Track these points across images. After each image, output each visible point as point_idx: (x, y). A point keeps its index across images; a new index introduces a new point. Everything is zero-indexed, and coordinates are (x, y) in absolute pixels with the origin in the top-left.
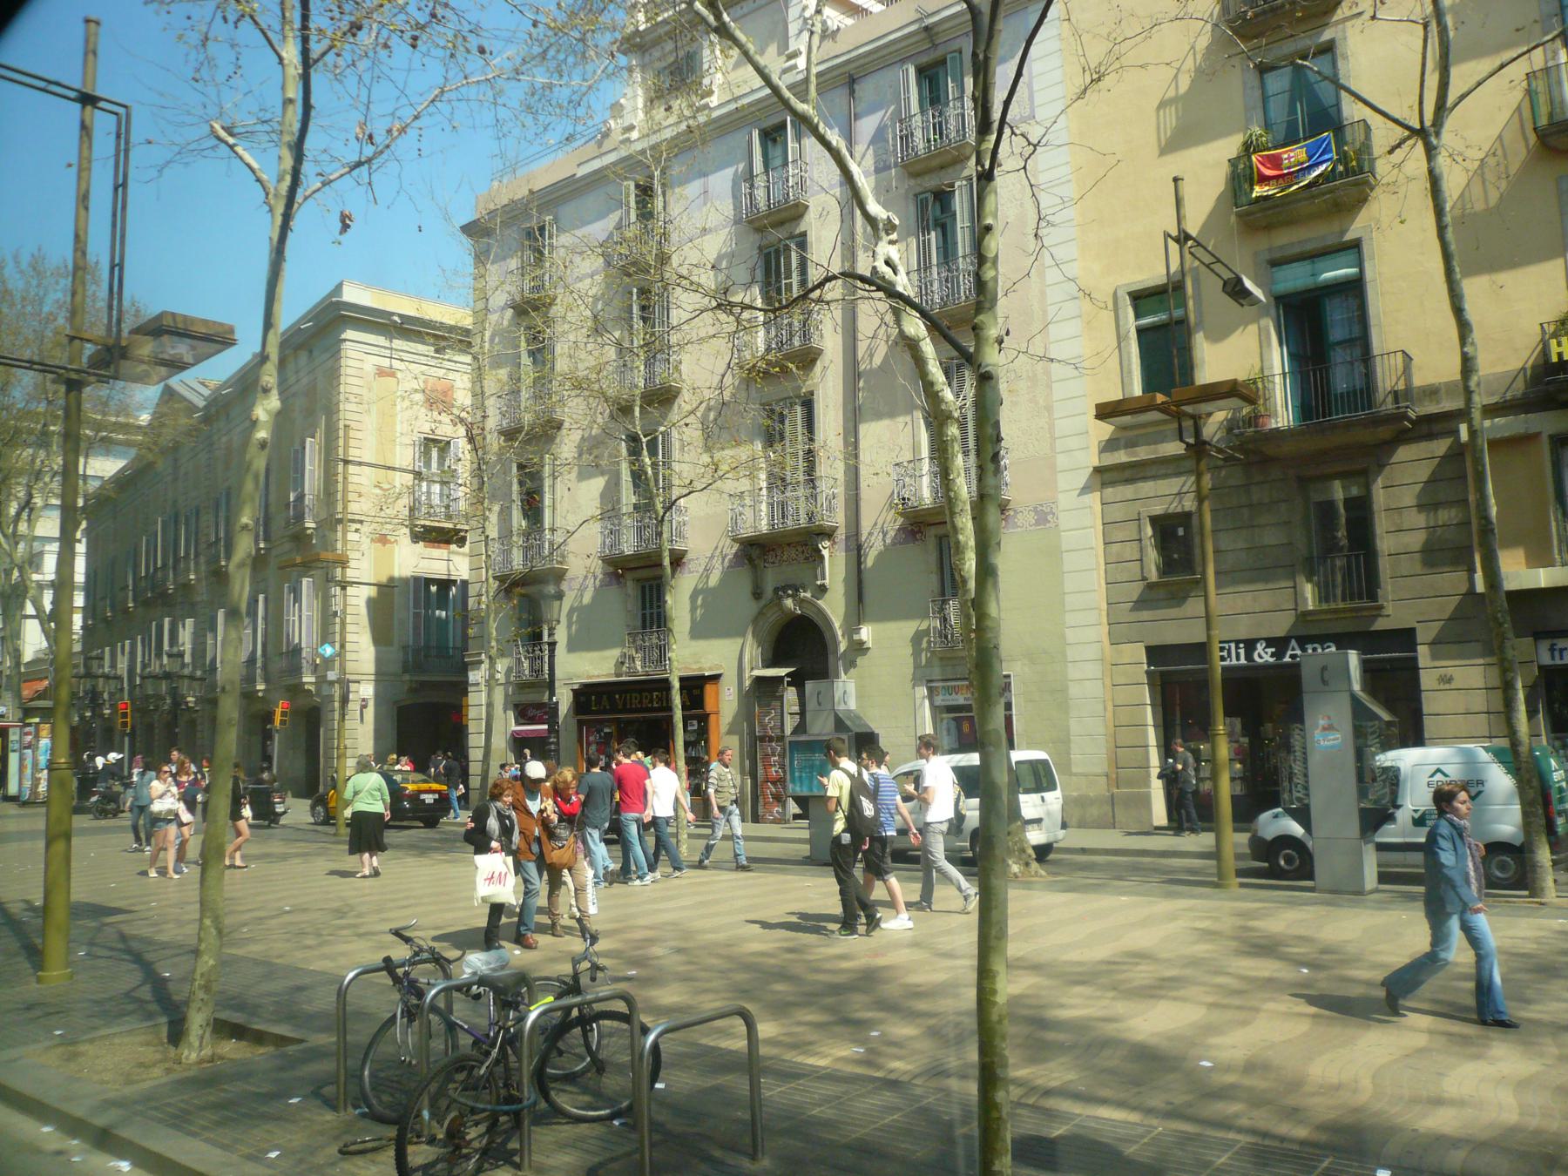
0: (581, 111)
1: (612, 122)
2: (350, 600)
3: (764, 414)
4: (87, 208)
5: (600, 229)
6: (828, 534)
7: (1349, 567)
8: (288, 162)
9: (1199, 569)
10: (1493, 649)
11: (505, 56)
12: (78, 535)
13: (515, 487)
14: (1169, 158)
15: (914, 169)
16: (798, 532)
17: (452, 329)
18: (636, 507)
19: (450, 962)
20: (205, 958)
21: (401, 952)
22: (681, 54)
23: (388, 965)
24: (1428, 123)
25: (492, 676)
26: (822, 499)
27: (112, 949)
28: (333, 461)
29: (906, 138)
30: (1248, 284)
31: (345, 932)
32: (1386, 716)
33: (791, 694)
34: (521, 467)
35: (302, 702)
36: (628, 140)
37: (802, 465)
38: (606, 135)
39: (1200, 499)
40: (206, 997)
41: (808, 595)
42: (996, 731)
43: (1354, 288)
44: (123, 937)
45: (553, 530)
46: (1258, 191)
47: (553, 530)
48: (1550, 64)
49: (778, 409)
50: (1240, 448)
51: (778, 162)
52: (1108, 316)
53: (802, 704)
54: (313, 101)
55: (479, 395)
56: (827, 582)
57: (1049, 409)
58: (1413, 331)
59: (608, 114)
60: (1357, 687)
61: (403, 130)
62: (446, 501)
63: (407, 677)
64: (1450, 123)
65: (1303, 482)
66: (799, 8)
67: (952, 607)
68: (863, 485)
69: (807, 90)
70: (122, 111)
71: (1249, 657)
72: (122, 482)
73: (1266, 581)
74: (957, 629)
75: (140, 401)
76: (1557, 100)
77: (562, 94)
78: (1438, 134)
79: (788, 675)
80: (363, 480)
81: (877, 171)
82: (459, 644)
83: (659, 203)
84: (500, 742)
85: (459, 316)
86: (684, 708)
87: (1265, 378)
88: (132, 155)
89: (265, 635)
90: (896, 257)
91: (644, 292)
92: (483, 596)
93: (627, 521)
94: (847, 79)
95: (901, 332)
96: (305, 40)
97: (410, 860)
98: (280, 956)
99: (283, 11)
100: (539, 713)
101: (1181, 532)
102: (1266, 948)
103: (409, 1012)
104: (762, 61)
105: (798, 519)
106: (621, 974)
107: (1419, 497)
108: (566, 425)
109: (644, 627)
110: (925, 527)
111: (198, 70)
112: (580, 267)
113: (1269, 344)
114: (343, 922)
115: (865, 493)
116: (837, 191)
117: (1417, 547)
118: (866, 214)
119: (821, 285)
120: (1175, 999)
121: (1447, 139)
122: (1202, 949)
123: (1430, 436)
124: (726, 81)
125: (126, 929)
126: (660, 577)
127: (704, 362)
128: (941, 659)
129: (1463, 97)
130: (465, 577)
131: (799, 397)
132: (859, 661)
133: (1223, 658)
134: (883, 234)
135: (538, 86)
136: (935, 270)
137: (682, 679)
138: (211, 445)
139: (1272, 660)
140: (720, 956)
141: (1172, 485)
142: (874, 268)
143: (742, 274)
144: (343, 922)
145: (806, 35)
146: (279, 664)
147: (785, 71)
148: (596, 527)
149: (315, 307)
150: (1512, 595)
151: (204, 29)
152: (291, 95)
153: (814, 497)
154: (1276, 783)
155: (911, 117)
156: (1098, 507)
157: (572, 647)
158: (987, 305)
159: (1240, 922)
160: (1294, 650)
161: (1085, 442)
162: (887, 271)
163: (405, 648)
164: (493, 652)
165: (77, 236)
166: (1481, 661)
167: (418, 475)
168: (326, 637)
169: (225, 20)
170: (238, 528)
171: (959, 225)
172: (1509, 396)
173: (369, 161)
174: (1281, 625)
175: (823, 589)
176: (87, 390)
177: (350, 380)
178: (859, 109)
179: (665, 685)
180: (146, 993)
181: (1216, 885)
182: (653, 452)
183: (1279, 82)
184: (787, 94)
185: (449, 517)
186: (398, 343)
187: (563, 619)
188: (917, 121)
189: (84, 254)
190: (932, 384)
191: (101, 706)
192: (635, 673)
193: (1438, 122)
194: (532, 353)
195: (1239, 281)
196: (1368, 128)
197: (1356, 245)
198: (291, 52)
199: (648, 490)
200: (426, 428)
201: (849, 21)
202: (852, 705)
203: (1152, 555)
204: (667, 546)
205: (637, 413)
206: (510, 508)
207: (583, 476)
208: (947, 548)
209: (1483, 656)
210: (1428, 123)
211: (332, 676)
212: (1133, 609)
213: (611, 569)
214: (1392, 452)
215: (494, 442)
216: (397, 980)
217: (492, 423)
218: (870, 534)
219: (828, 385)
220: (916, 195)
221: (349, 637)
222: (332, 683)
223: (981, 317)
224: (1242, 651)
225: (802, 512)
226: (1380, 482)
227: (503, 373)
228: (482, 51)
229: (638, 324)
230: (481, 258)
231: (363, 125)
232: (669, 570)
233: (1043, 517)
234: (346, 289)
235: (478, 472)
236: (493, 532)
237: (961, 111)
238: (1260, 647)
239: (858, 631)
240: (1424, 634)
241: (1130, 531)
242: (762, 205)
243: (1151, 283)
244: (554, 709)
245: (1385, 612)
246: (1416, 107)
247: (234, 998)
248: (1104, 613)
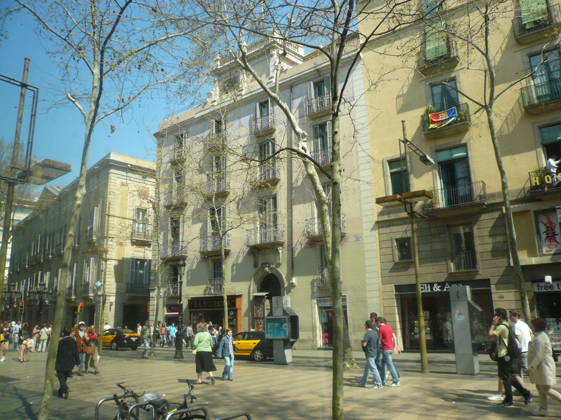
0: (197, 95)
2: (108, 266)
4: (21, 123)
6: (281, 244)
7: (466, 257)
8: (93, 107)
9: (413, 258)
10: (518, 287)
11: (172, 73)
12: (9, 241)
13: (169, 225)
14: (400, 115)
15: (313, 117)
17: (148, 169)
19: (139, 397)
20: (46, 395)
21: (120, 393)
22: (232, 77)
23: (115, 398)
24: (487, 104)
25: (159, 294)
26: (279, 232)
27: (11, 393)
28: (104, 215)
29: (310, 106)
30: (428, 157)
31: (100, 388)
32: (480, 309)
33: (267, 302)
34: (172, 218)
35: (88, 303)
36: (213, 105)
37: (272, 219)
38: (206, 103)
39: (413, 232)
40: (46, 410)
41: (274, 266)
42: (339, 308)
43: (465, 160)
44: (15, 389)
45: (183, 242)
46: (432, 126)
48: (528, 85)
49: (264, 199)
50: (427, 215)
51: (265, 114)
52: (380, 167)
54: (103, 87)
55: (158, 193)
56: (281, 261)
57: (360, 201)
58: (485, 175)
60: (469, 299)
61: (134, 98)
62: (144, 230)
63: (127, 295)
64: (495, 104)
65: (449, 226)
66: (274, 62)
67: (326, 271)
68: (294, 227)
70: (35, 90)
71: (431, 289)
72: (26, 222)
74: (327, 279)
75: (35, 192)
76: (531, 97)
78: (491, 107)
79: (266, 295)
80: (115, 222)
81: (300, 117)
82: (147, 283)
83: (223, 127)
84: (161, 318)
85: (151, 165)
86: (228, 307)
87: (435, 190)
88: (38, 104)
89: (76, 279)
90: (306, 146)
91: (218, 158)
92: (156, 266)
93: (210, 239)
94: (290, 86)
95: (308, 172)
96: (102, 66)
97: (125, 361)
98: (74, 397)
99: (94, 56)
101: (407, 244)
102: (440, 394)
103: (122, 415)
104: (260, 79)
105: (270, 239)
106: (202, 403)
107: (489, 232)
109: (215, 277)
110: (315, 242)
111: (63, 77)
112: (195, 149)
113: (436, 179)
114: (99, 384)
117: (490, 250)
118: (296, 132)
119: (279, 152)
120: (406, 412)
121: (494, 109)
122: (416, 394)
123: (493, 211)
124: (248, 86)
125: (17, 386)
129: (499, 95)
130: (150, 258)
133: (422, 290)
134: (301, 138)
136: (320, 152)
138: (60, 209)
139: (440, 290)
140: (240, 397)
141: (404, 227)
143: (252, 150)
144: (99, 384)
145: (276, 71)
146: (81, 289)
147: (268, 83)
148: (198, 241)
150: (524, 267)
151: (67, 62)
152: (95, 85)
153: (276, 231)
154: (442, 335)
156: (377, 235)
157: (188, 284)
158: (336, 159)
159: (430, 385)
160: (447, 286)
161: (372, 212)
165: (17, 132)
166: (513, 291)
167: (134, 221)
168: (98, 279)
169: (74, 59)
170: (68, 235)
171: (328, 136)
172: (519, 197)
173: (122, 108)
174: (443, 278)
175: (279, 265)
176: (16, 187)
177: (112, 181)
179: (222, 298)
180: (23, 410)
181: (422, 372)
182: (219, 214)
183: (437, 90)
184: (268, 90)
185: (145, 236)
186: (129, 174)
187: (185, 273)
188: (314, 101)
189: (19, 138)
190: (318, 191)
191: (13, 303)
192: (211, 294)
193: (491, 103)
194: (177, 179)
195: (425, 156)
196: (468, 106)
197: (465, 145)
198: (97, 71)
200: (138, 205)
201: (291, 67)
203: (397, 253)
204: (223, 248)
205: (214, 200)
207: (194, 223)
208: (323, 248)
209: (514, 289)
210: (487, 104)
211: (100, 293)
212: (390, 272)
213: (203, 256)
214: (480, 216)
215: (162, 210)
216: (118, 403)
217: (162, 202)
218: (296, 245)
219: (282, 192)
220: (313, 126)
221: (107, 280)
222: (100, 296)
223: (333, 163)
224: (429, 287)
225: (272, 236)
226: (476, 227)
227: (167, 186)
228: (163, 70)
229: (215, 169)
230: (160, 145)
231: (120, 96)
233: (358, 239)
234: (111, 155)
235: (157, 220)
236: (161, 242)
237: (327, 97)
238: (435, 286)
239: (291, 279)
240: (493, 281)
241: (389, 244)
243: (394, 158)
244: (181, 306)
245: (479, 273)
246: (483, 98)
247: (56, 412)
248: (380, 274)
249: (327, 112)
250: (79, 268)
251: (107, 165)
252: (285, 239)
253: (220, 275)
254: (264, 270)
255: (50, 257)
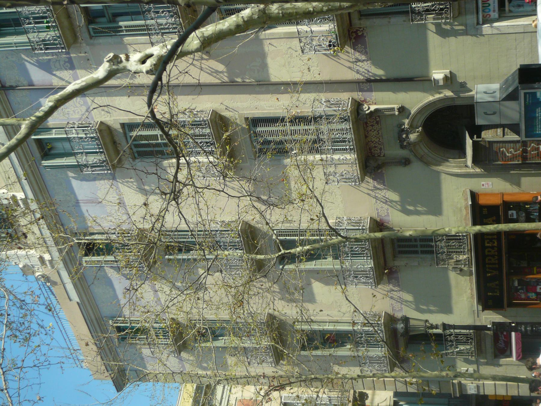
0: (28, 299)
1: (37, 274)
3: (262, 158)
5: (120, 283)
6: (358, 106)
13: (319, 353)
18: (336, 257)
25: (471, 376)
26: (330, 111)
29: (47, 45)
33: (487, 135)
34: (303, 348)
36: (51, 262)
37: (302, 127)
41: (407, 121)
45: (354, 324)
47: (354, 324)
51: (67, 145)
53: (496, 126)
55: (248, 380)
56: (396, 106)
59: (31, 278)
68: (318, 78)
69: (12, 125)
77: (15, 314)
79: (472, 137)
81: (72, 67)
85: (186, 396)
86: (498, 222)
91: (168, 249)
95: (197, 50)
100: (502, 338)
108: (271, 311)
109: (432, 252)
112: (153, 299)
115: (325, 77)
116: (88, 100)
126: (392, 240)
127: (219, 204)
128: (460, 14)
130: (391, 394)
131: (249, 130)
132: (461, 80)
134: (121, 66)
135: (9, 333)
136: (149, 22)
137: (475, 224)
142: (148, 72)
148: (352, 289)
153: (328, 117)
155: (30, 41)
157: (447, 309)
162: (149, 63)
164: (451, 374)
175: (402, 110)
178: (25, 83)
179: (479, 237)
182: (291, 244)
184: (14, 141)
188: (33, 36)
194: (216, 337)
199: (323, 248)
202: (496, 86)
204: (367, 234)
205: (262, 257)
206: (336, 357)
207: (312, 299)
213: (385, 278)
217: (269, 369)
218: (358, 72)
219: (241, 106)
220: (91, 37)
225: (339, 127)
227: (231, 360)
230: (142, 377)
232: (385, 233)
236: (355, 371)
239: (436, 81)
242: (102, 157)
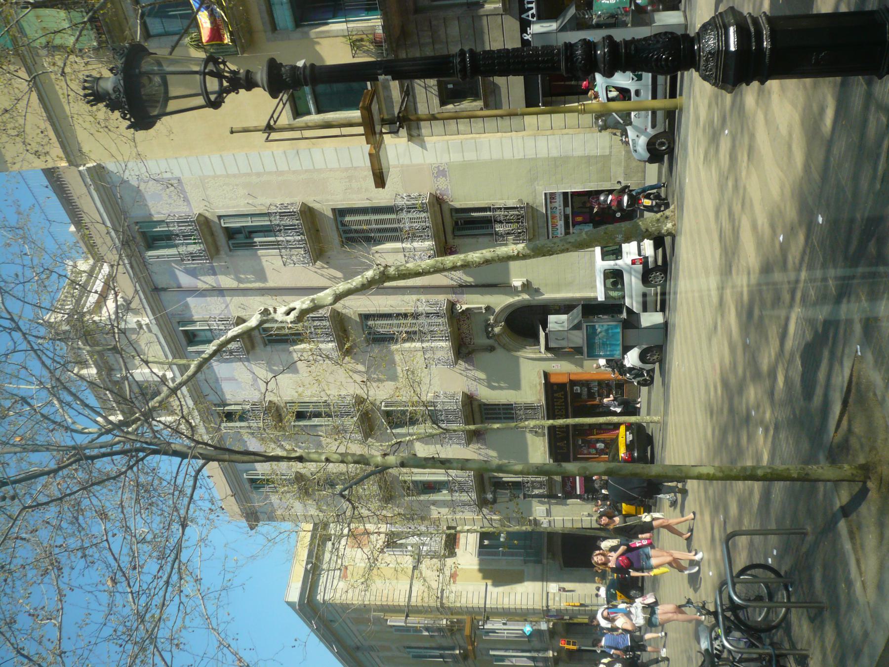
6: (452, 305)
15: (213, 251)
16: (451, 324)
29: (193, 256)
35: (560, 629)
41: (492, 318)
46: (227, 40)
56: (483, 306)
63: (545, 561)
69: (184, 365)
73: (482, 33)
86: (567, 417)
87: (348, 35)
105: (442, 325)
134: (270, 317)
146: (536, 643)
149: (301, 617)
155: (180, 254)
156: (434, 138)
163: (525, 562)
171: (250, 224)
175: (488, 309)
178: (175, 285)
184: (185, 377)
188: (182, 249)
218: (452, 279)
220: (230, 250)
233: (441, 172)
234: (290, 599)
248: (504, 134)
249: (203, 227)
250: (498, 646)
251: (310, 608)
252: (442, 299)
253: (507, 409)
254: (498, 335)
255: (457, 652)
